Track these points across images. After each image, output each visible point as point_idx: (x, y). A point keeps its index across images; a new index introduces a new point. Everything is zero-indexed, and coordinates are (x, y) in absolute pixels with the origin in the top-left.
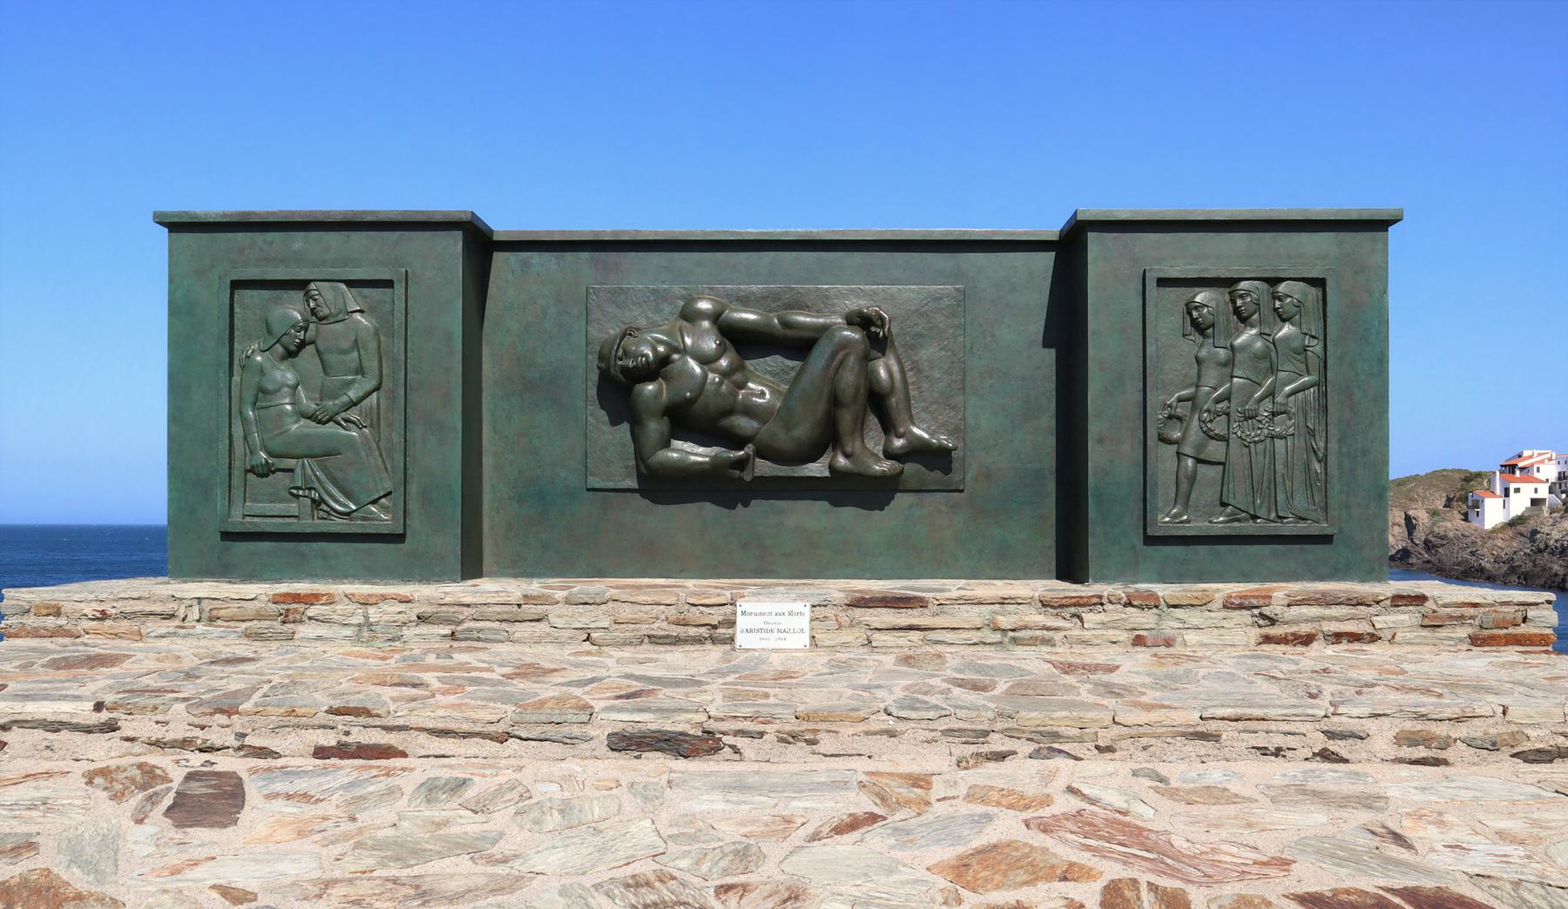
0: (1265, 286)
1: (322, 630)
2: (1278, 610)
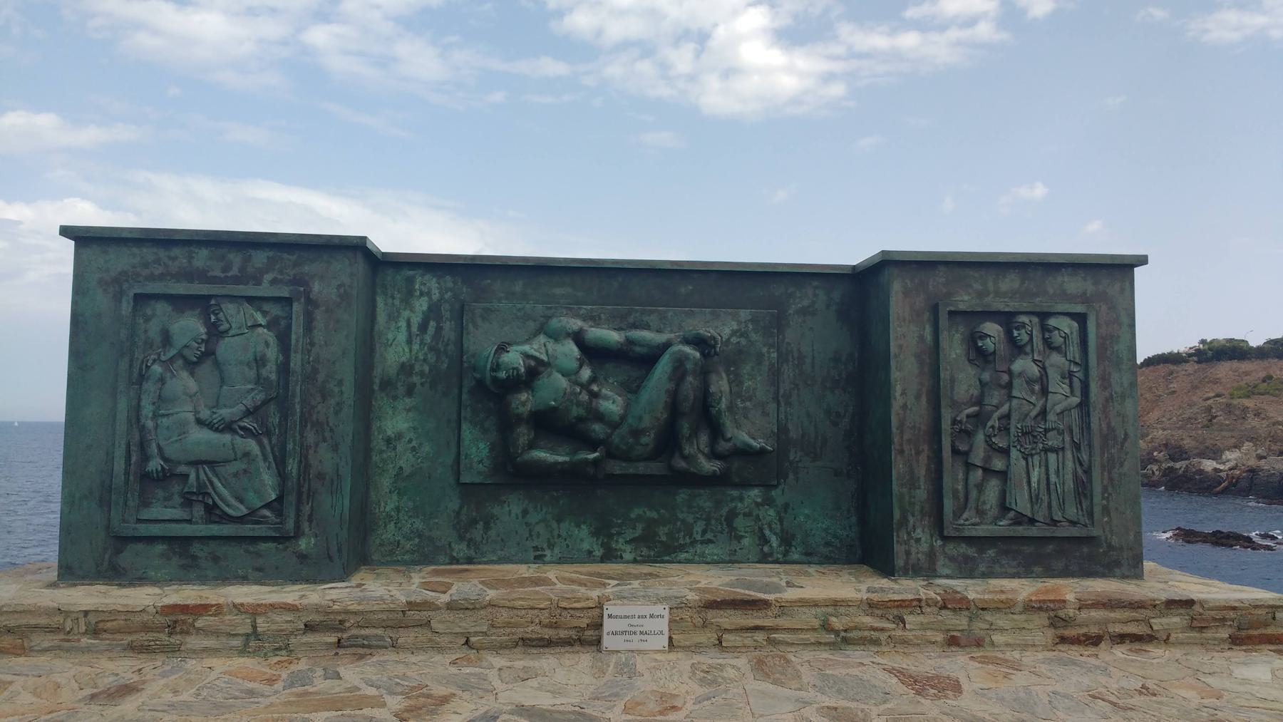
0: (1035, 320)
1: (210, 642)
2: (1071, 612)
